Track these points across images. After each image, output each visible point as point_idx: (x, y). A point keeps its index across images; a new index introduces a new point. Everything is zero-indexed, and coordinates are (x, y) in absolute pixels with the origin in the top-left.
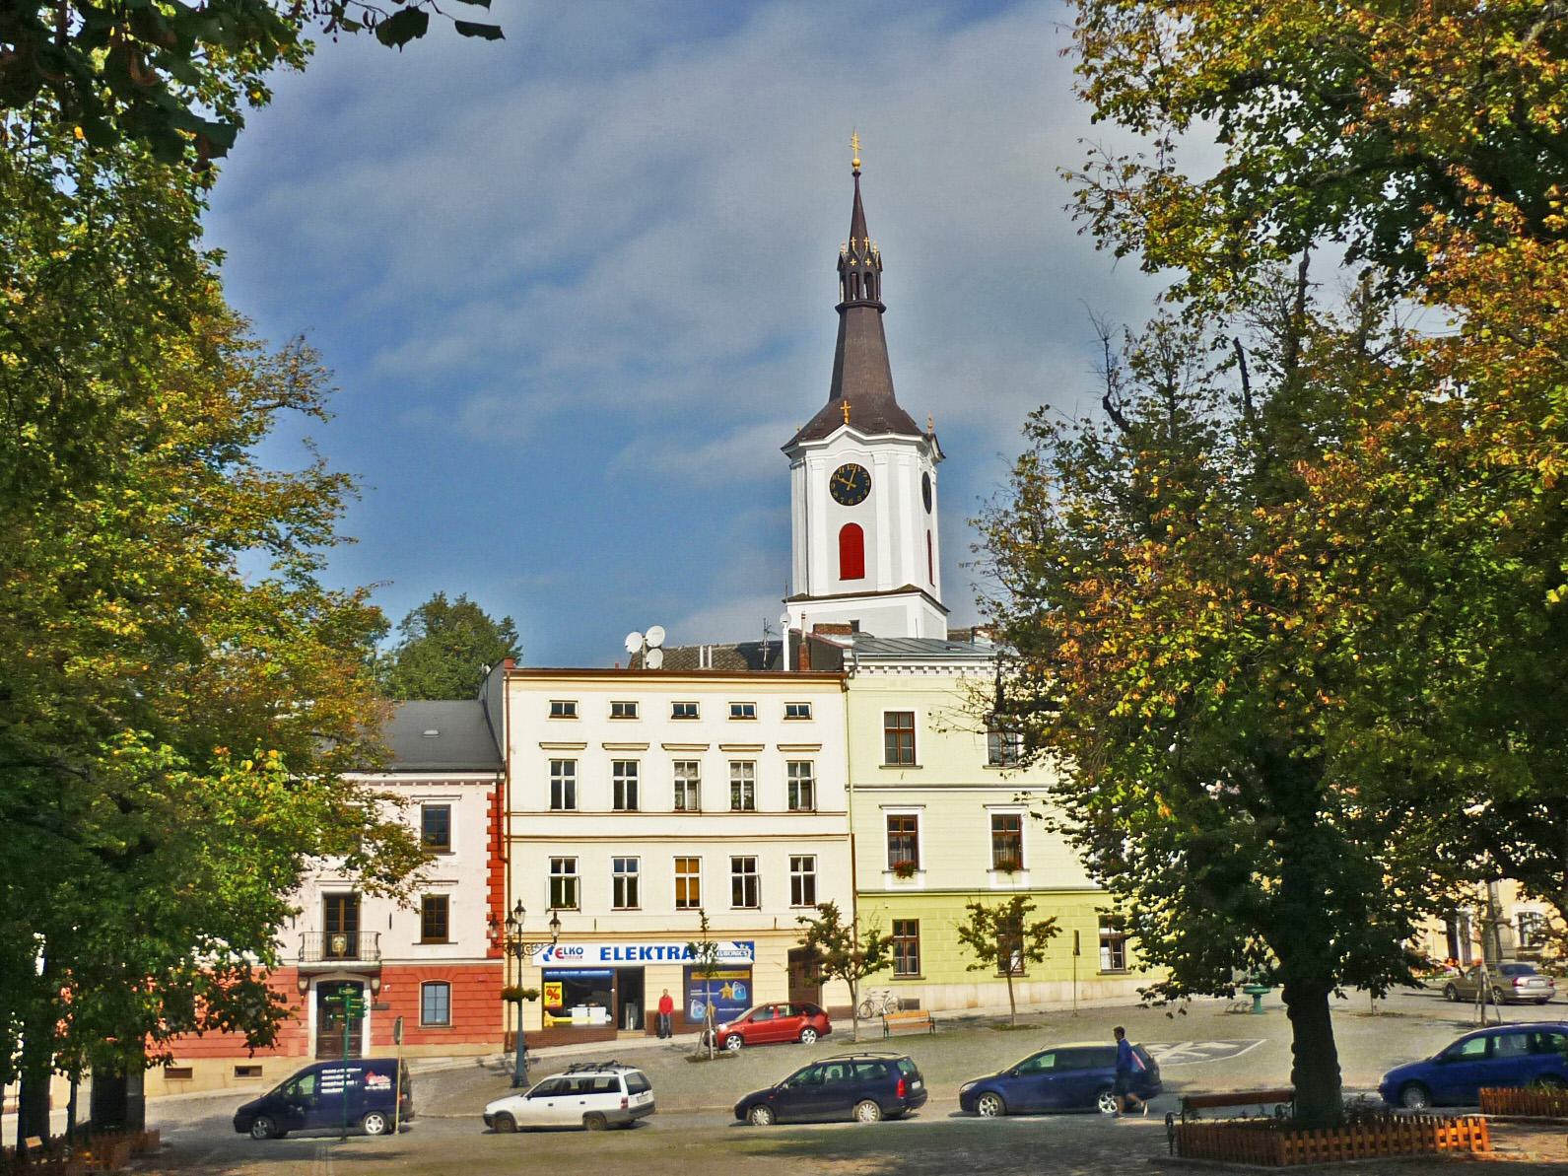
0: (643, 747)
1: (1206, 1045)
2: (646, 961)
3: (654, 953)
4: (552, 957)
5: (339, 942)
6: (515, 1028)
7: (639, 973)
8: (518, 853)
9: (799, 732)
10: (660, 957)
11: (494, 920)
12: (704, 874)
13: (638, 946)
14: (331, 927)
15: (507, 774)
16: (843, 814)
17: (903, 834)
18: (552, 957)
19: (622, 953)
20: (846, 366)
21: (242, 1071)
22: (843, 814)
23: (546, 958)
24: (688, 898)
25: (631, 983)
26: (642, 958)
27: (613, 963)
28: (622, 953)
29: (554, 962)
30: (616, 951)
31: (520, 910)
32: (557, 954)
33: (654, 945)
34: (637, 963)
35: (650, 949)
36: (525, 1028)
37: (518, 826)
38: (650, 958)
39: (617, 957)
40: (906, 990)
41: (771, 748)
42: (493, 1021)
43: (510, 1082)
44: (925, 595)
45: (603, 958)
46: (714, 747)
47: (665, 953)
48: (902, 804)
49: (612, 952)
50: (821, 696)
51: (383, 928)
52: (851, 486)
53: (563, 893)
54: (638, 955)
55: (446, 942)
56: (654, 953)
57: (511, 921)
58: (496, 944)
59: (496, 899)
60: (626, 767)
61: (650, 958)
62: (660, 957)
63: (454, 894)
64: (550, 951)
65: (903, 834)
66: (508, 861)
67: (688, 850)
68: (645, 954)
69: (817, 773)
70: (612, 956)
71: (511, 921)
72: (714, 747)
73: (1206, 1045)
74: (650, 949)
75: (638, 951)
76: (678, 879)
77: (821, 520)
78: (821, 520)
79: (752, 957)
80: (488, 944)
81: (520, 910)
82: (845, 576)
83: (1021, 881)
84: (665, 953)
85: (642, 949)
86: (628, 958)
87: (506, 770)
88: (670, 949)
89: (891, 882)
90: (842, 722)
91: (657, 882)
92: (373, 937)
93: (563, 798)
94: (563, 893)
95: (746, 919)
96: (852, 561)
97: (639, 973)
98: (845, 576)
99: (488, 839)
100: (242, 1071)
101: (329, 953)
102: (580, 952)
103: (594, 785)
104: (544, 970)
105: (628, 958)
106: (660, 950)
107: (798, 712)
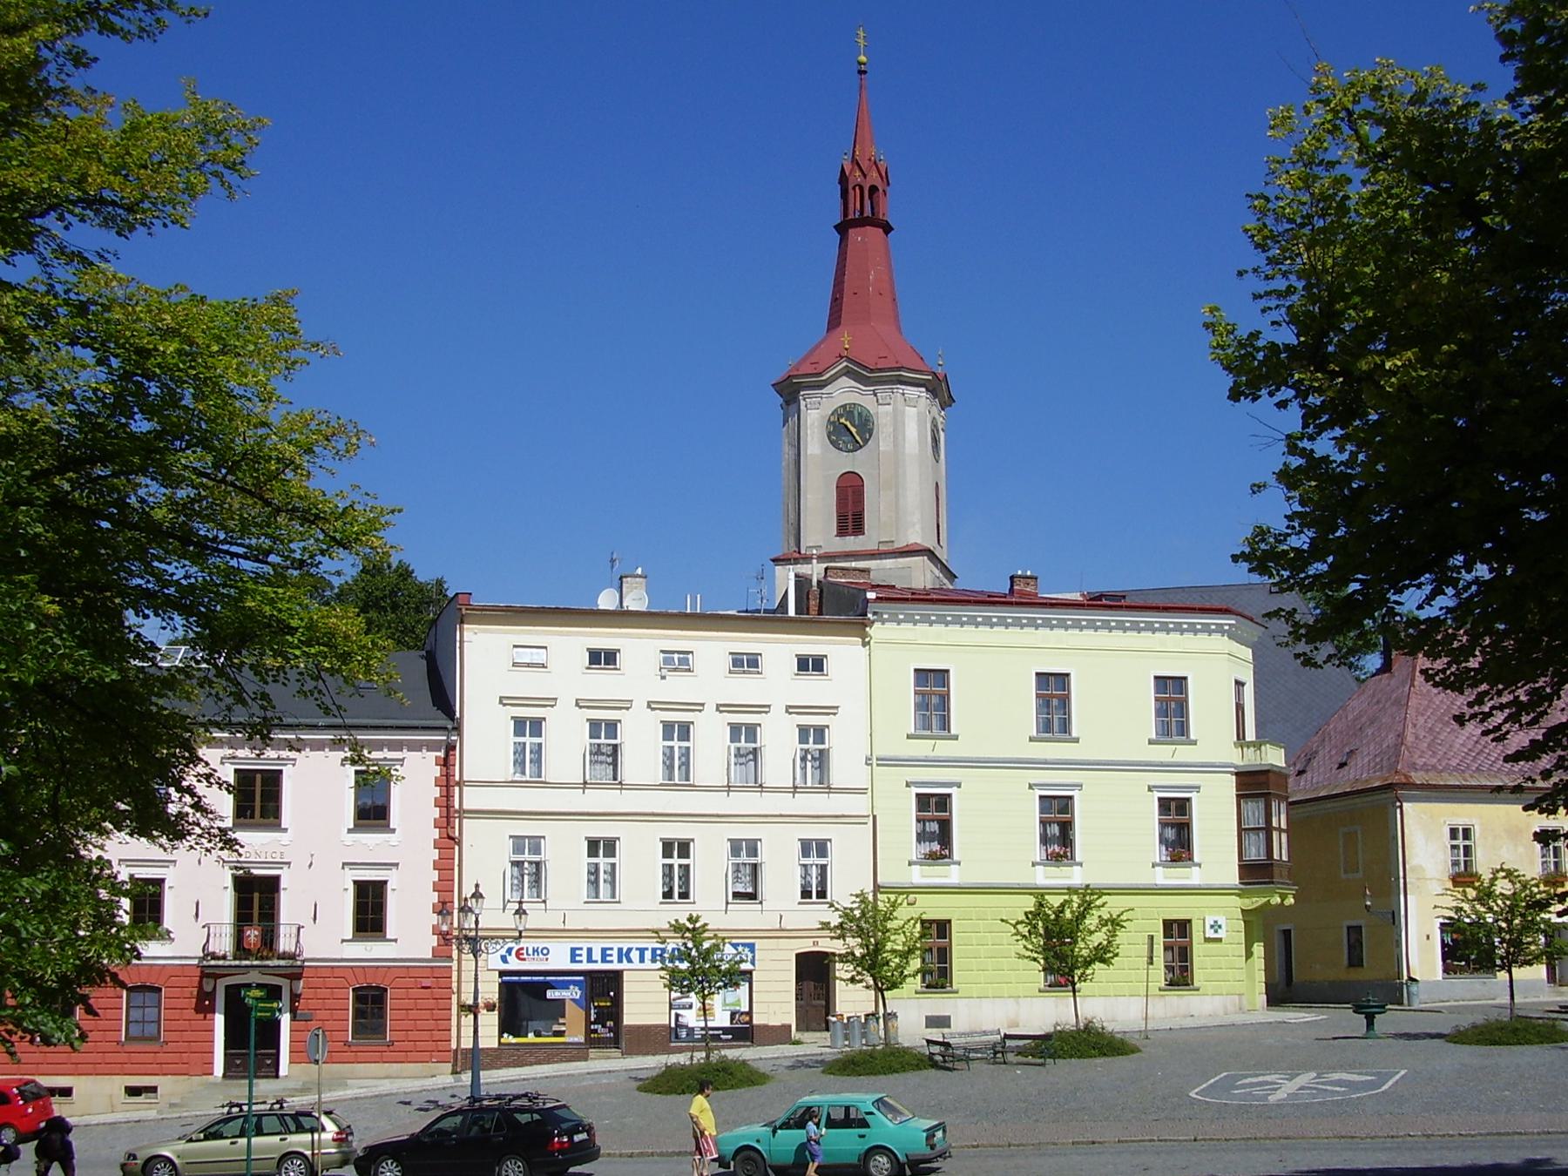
0: (625, 705)
1: (1336, 1076)
2: (625, 965)
3: (635, 955)
4: (512, 959)
5: (253, 934)
6: (467, 1043)
7: (616, 976)
8: (471, 830)
9: (811, 690)
10: (642, 960)
11: (442, 909)
12: (696, 860)
13: (615, 945)
14: (243, 916)
15: (460, 735)
16: (862, 791)
17: (935, 814)
18: (512, 959)
19: (597, 955)
20: (847, 298)
21: (133, 1091)
22: (862, 791)
23: (504, 959)
24: (677, 886)
25: (604, 988)
26: (620, 961)
27: (585, 966)
28: (597, 955)
29: (514, 964)
30: (590, 951)
31: (477, 895)
32: (518, 954)
33: (635, 946)
34: (615, 966)
35: (630, 950)
36: (463, 1046)
37: (472, 799)
38: (630, 961)
39: (590, 960)
40: (937, 1004)
41: (778, 710)
42: (437, 1035)
43: (1455, 726)
44: (929, 553)
45: (573, 960)
46: (710, 708)
47: (648, 955)
48: (934, 778)
49: (584, 953)
50: (839, 650)
51: (306, 920)
52: (851, 430)
53: (530, 872)
54: (615, 958)
55: (384, 939)
56: (635, 955)
57: (465, 910)
58: (445, 938)
59: (444, 886)
60: (604, 729)
61: (630, 961)
62: (642, 960)
63: (393, 879)
64: (509, 951)
65: (935, 814)
66: (459, 843)
67: (677, 831)
68: (624, 955)
69: (833, 740)
70: (584, 958)
71: (465, 910)
72: (710, 708)
73: (1336, 1076)
74: (630, 950)
75: (615, 953)
76: (688, 857)
77: (822, 463)
78: (822, 463)
79: (753, 963)
80: (434, 941)
81: (477, 895)
82: (842, 531)
83: (1073, 876)
84: (648, 955)
85: (620, 950)
86: (604, 960)
87: (458, 729)
88: (654, 950)
89: (920, 875)
90: (868, 673)
91: (640, 863)
92: (294, 930)
93: (529, 761)
94: (530, 872)
95: (744, 917)
96: (851, 519)
97: (616, 976)
98: (842, 531)
99: (436, 813)
100: (133, 1091)
101: (241, 948)
102: (545, 952)
103: (566, 743)
104: (502, 973)
105: (604, 960)
106: (642, 951)
107: (811, 665)
